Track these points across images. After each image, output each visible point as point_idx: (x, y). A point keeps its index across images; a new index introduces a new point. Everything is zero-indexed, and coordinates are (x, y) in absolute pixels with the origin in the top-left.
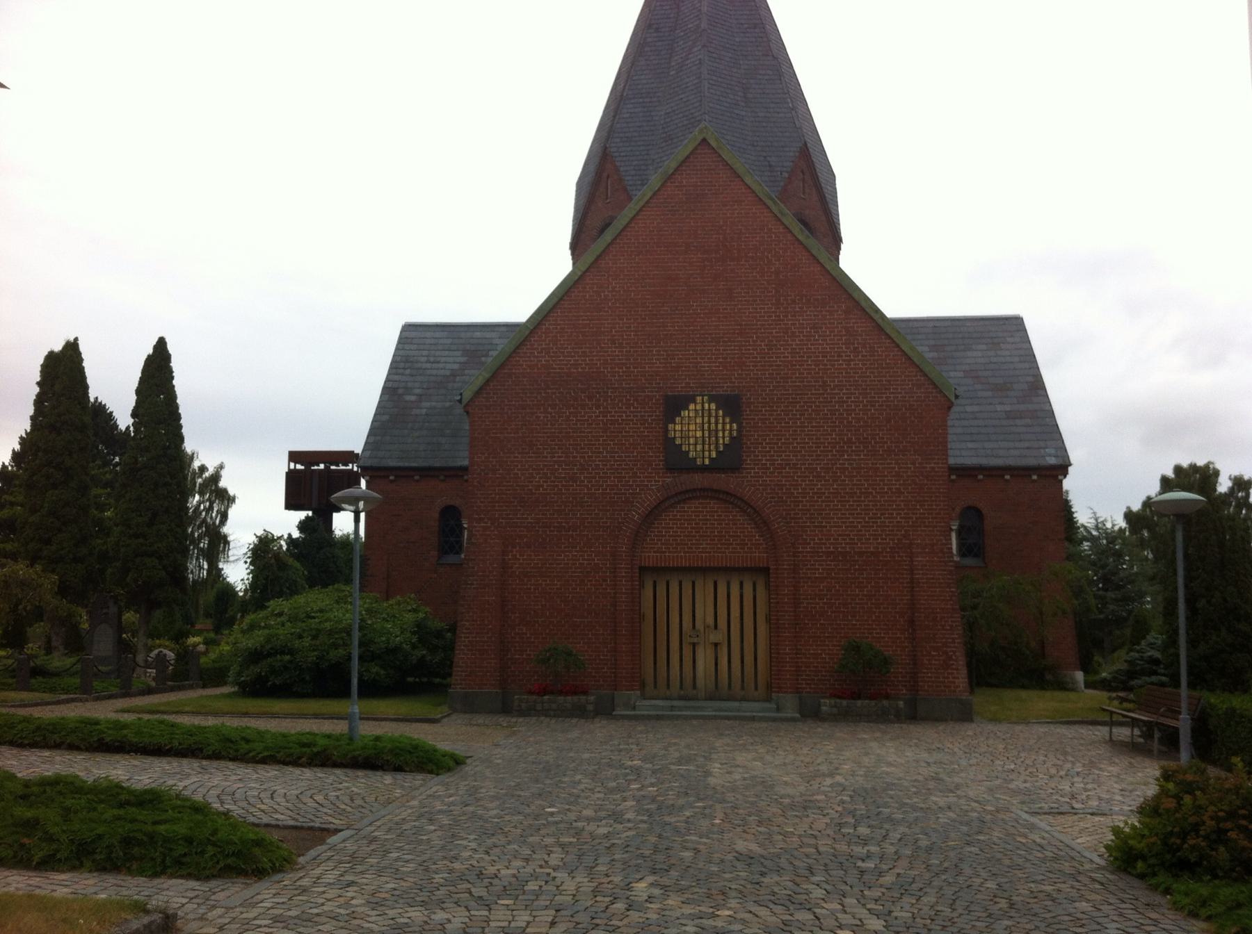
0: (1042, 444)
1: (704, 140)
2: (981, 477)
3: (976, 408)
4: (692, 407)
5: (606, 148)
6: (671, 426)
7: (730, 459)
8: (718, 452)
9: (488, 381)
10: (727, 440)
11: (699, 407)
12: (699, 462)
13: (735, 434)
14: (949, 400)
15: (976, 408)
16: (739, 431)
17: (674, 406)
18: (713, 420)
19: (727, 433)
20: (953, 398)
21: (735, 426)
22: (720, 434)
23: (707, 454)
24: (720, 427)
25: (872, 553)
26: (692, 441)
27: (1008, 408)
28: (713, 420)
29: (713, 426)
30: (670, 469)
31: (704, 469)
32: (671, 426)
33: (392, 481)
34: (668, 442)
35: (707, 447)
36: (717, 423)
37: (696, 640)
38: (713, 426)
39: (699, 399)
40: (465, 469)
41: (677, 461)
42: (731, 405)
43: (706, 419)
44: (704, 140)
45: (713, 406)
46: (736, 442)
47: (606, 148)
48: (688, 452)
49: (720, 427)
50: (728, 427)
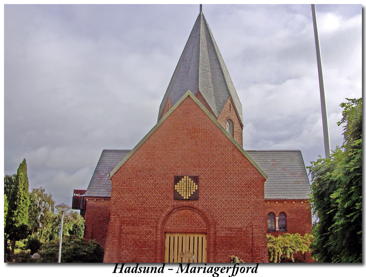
0: (305, 192)
1: (189, 96)
2: (285, 203)
3: (285, 180)
4: (183, 179)
5: (130, 151)
6: (176, 186)
7: (195, 197)
8: (191, 195)
9: (118, 170)
10: (194, 191)
11: (185, 180)
12: (185, 198)
13: (197, 189)
14: (265, 178)
15: (285, 180)
16: (198, 188)
17: (177, 179)
18: (190, 184)
19: (194, 188)
20: (266, 178)
21: (197, 186)
22: (192, 189)
23: (187, 195)
24: (192, 186)
25: (240, 228)
26: (182, 191)
27: (295, 180)
28: (190, 184)
29: (190, 186)
30: (175, 199)
31: (186, 200)
32: (176, 186)
33: (95, 201)
34: (175, 191)
35: (187, 193)
36: (191, 185)
37: (182, 256)
38: (190, 186)
39: (185, 177)
40: (110, 198)
41: (178, 197)
42: (196, 179)
43: (187, 184)
44: (189, 96)
45: (190, 179)
46: (197, 191)
47: (130, 151)
48: (181, 195)
49: (192, 186)
50: (194, 186)
